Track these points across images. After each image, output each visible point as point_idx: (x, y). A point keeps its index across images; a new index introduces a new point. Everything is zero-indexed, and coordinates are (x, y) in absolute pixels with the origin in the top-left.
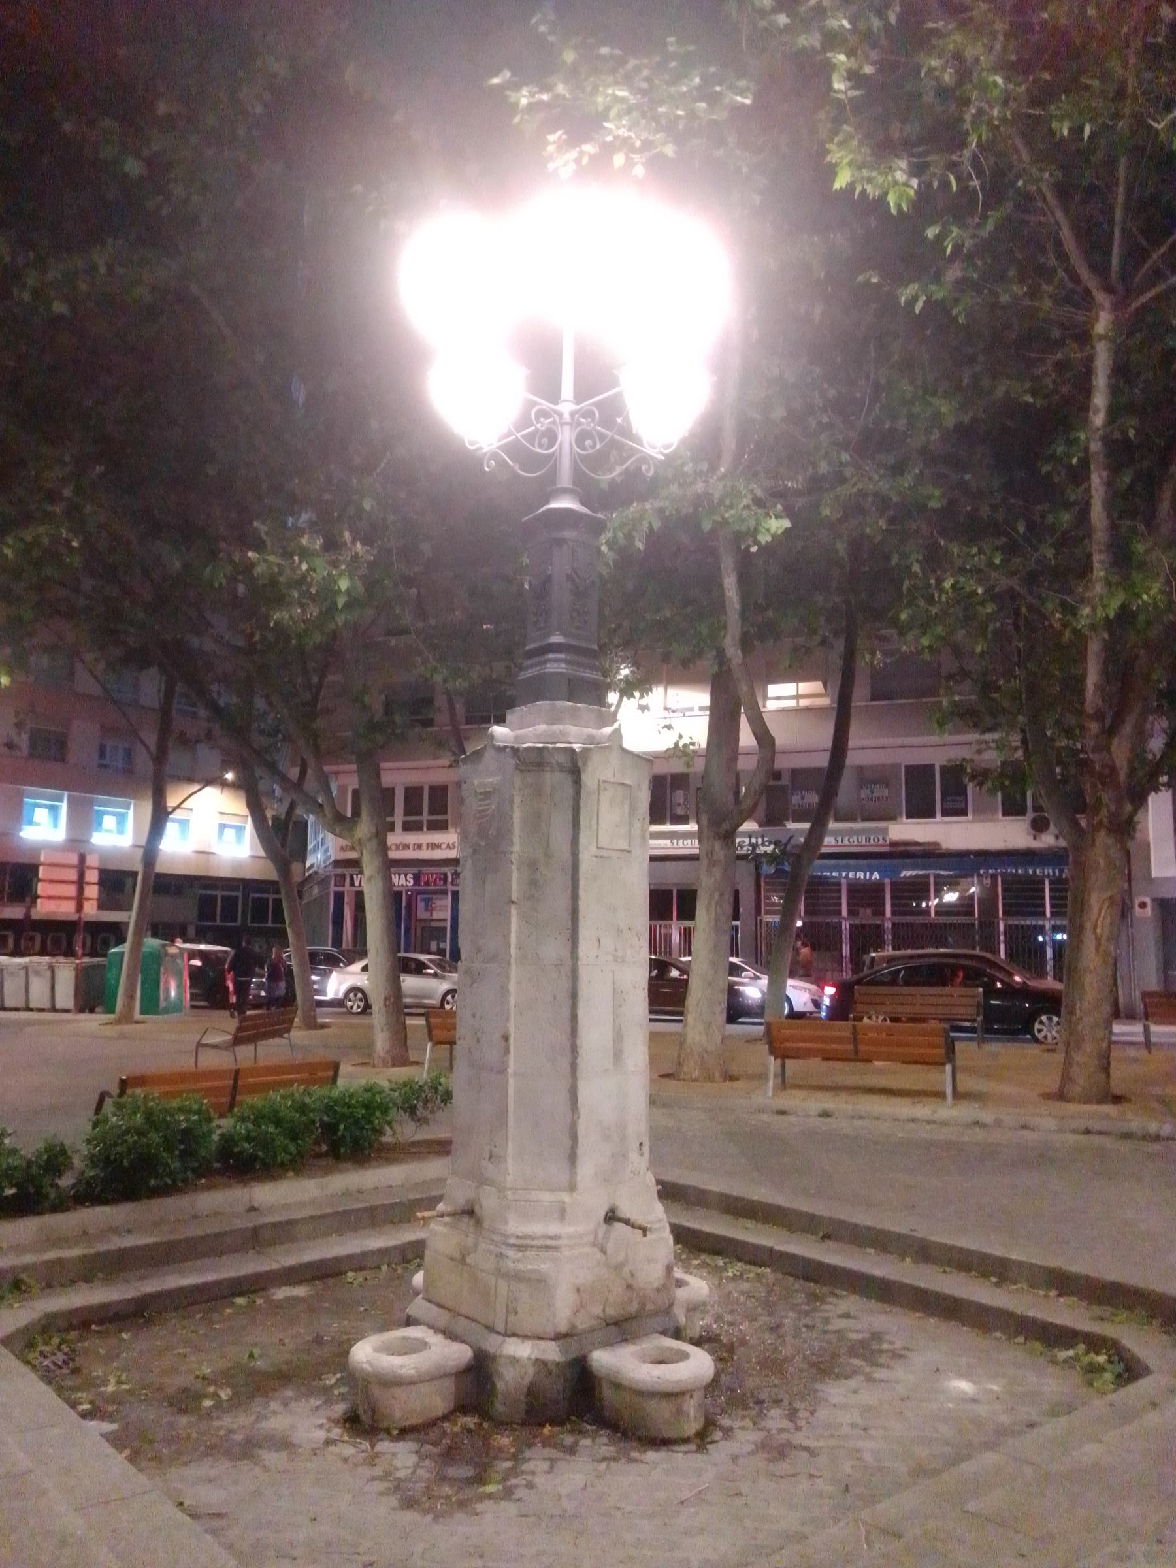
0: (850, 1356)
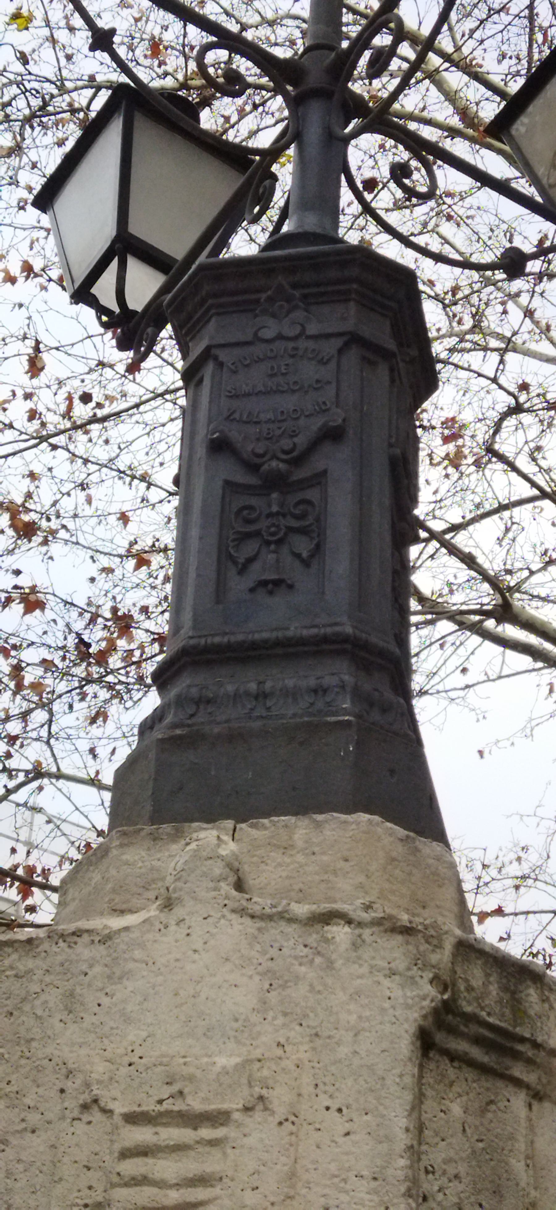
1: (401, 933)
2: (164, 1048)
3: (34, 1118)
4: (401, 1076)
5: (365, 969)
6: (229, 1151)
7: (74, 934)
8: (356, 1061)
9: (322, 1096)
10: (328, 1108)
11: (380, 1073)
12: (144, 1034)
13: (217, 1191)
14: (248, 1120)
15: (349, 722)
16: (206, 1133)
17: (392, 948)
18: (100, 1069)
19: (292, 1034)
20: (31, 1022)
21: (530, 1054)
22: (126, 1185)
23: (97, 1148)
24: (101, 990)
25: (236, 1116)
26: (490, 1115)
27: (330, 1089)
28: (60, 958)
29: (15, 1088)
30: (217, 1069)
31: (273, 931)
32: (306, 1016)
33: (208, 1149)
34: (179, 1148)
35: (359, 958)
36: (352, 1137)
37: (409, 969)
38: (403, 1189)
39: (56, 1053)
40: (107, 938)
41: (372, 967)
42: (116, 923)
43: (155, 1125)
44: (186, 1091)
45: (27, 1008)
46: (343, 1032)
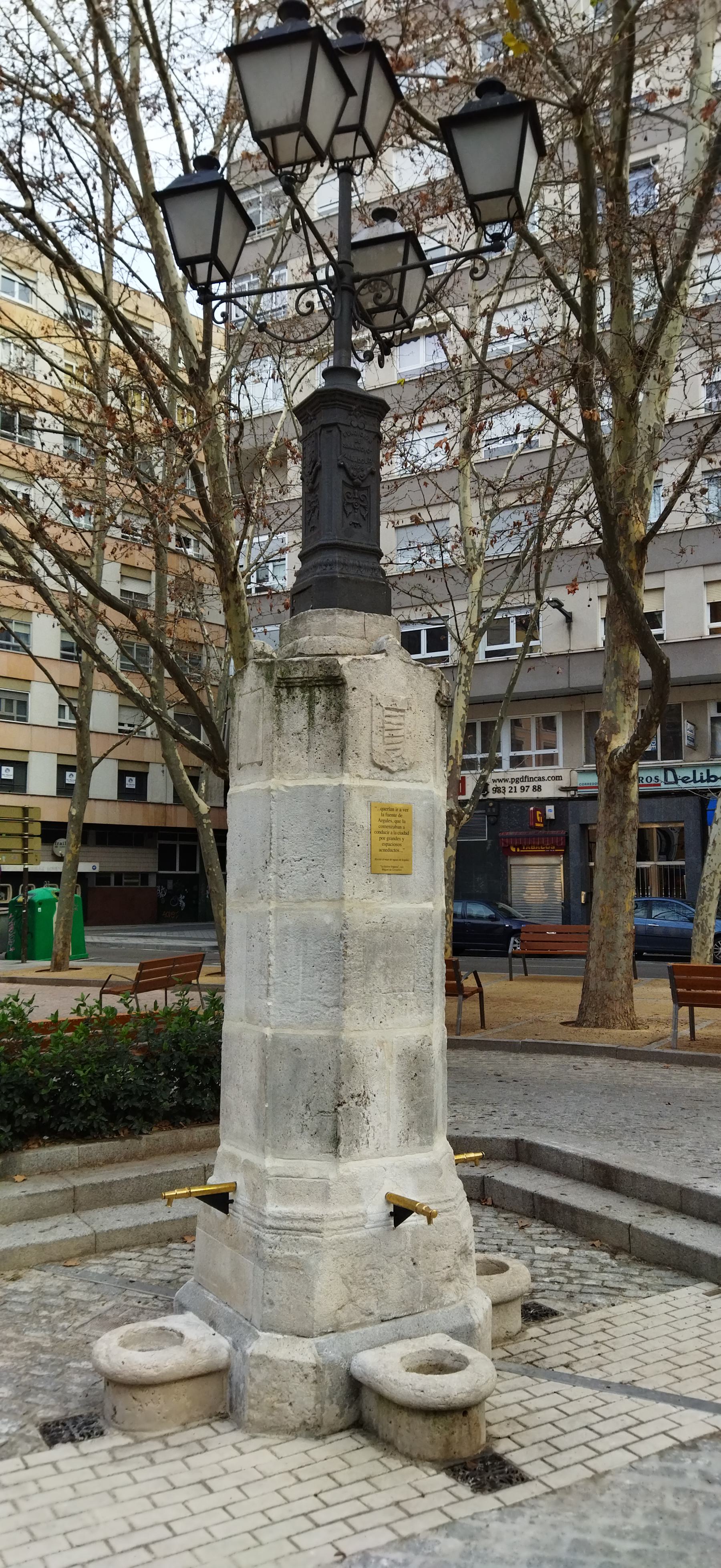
0: (218, 165)
18: (379, 696)
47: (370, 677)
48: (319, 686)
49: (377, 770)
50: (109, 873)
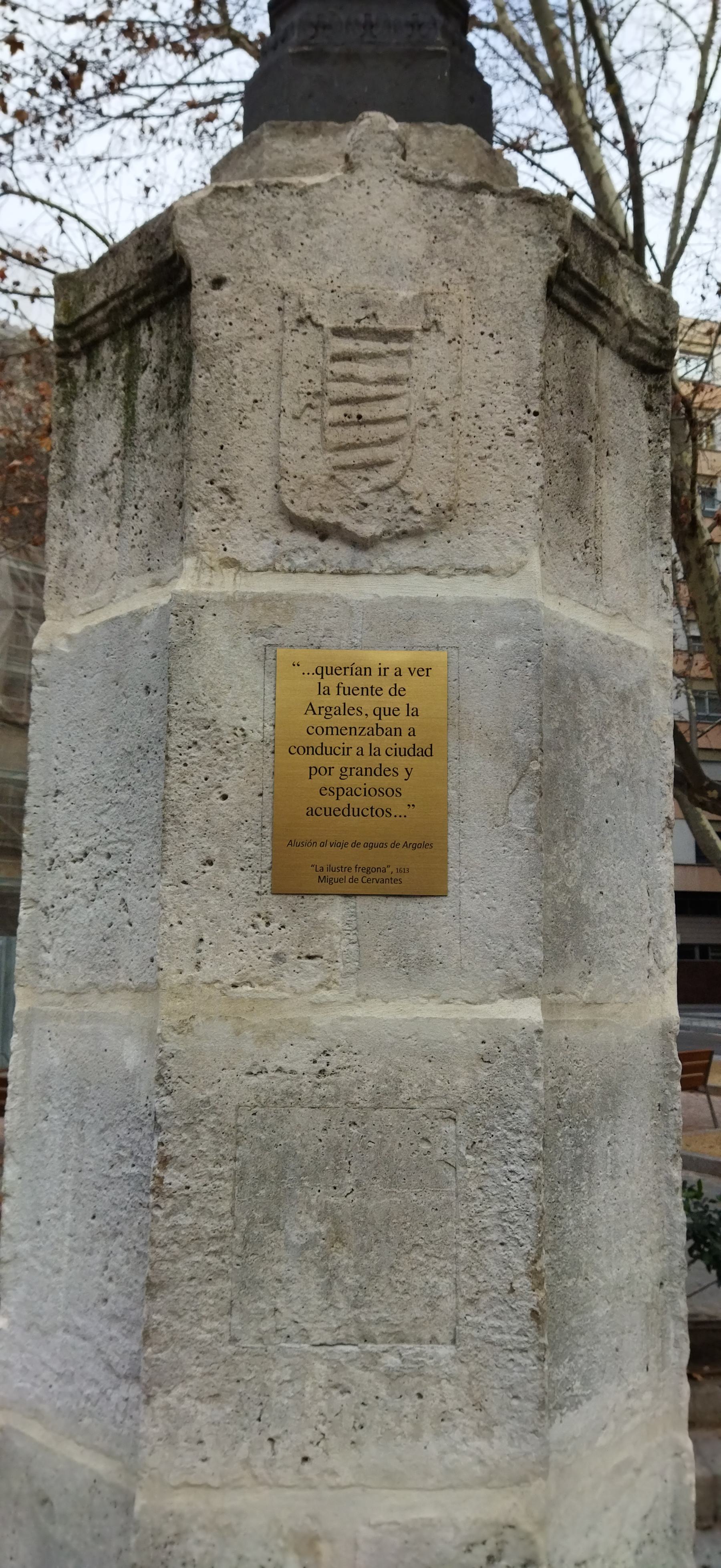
1: (535, 203)
2: (356, 281)
3: (259, 329)
4: (536, 312)
5: (506, 230)
6: (413, 360)
7: (276, 185)
8: (503, 300)
9: (478, 324)
10: (482, 333)
11: (520, 309)
12: (340, 270)
13: (405, 387)
14: (425, 338)
15: (443, 54)
16: (394, 346)
17: (528, 215)
18: (309, 294)
19: (454, 277)
20: (249, 253)
21: (605, 309)
22: (337, 380)
23: (313, 353)
24: (303, 232)
25: (417, 334)
26: (578, 351)
27: (484, 320)
28: (267, 204)
29: (242, 305)
30: (400, 298)
31: (435, 195)
32: (464, 263)
33: (396, 358)
34: (375, 356)
35: (503, 221)
36: (501, 354)
37: (540, 232)
38: (538, 393)
39: (271, 279)
40: (303, 192)
41: (513, 228)
42: (309, 181)
43: (355, 339)
44: (378, 313)
45: (244, 242)
46: (491, 277)
47: (280, 242)
48: (146, 314)
49: (302, 539)
50: (692, 946)
